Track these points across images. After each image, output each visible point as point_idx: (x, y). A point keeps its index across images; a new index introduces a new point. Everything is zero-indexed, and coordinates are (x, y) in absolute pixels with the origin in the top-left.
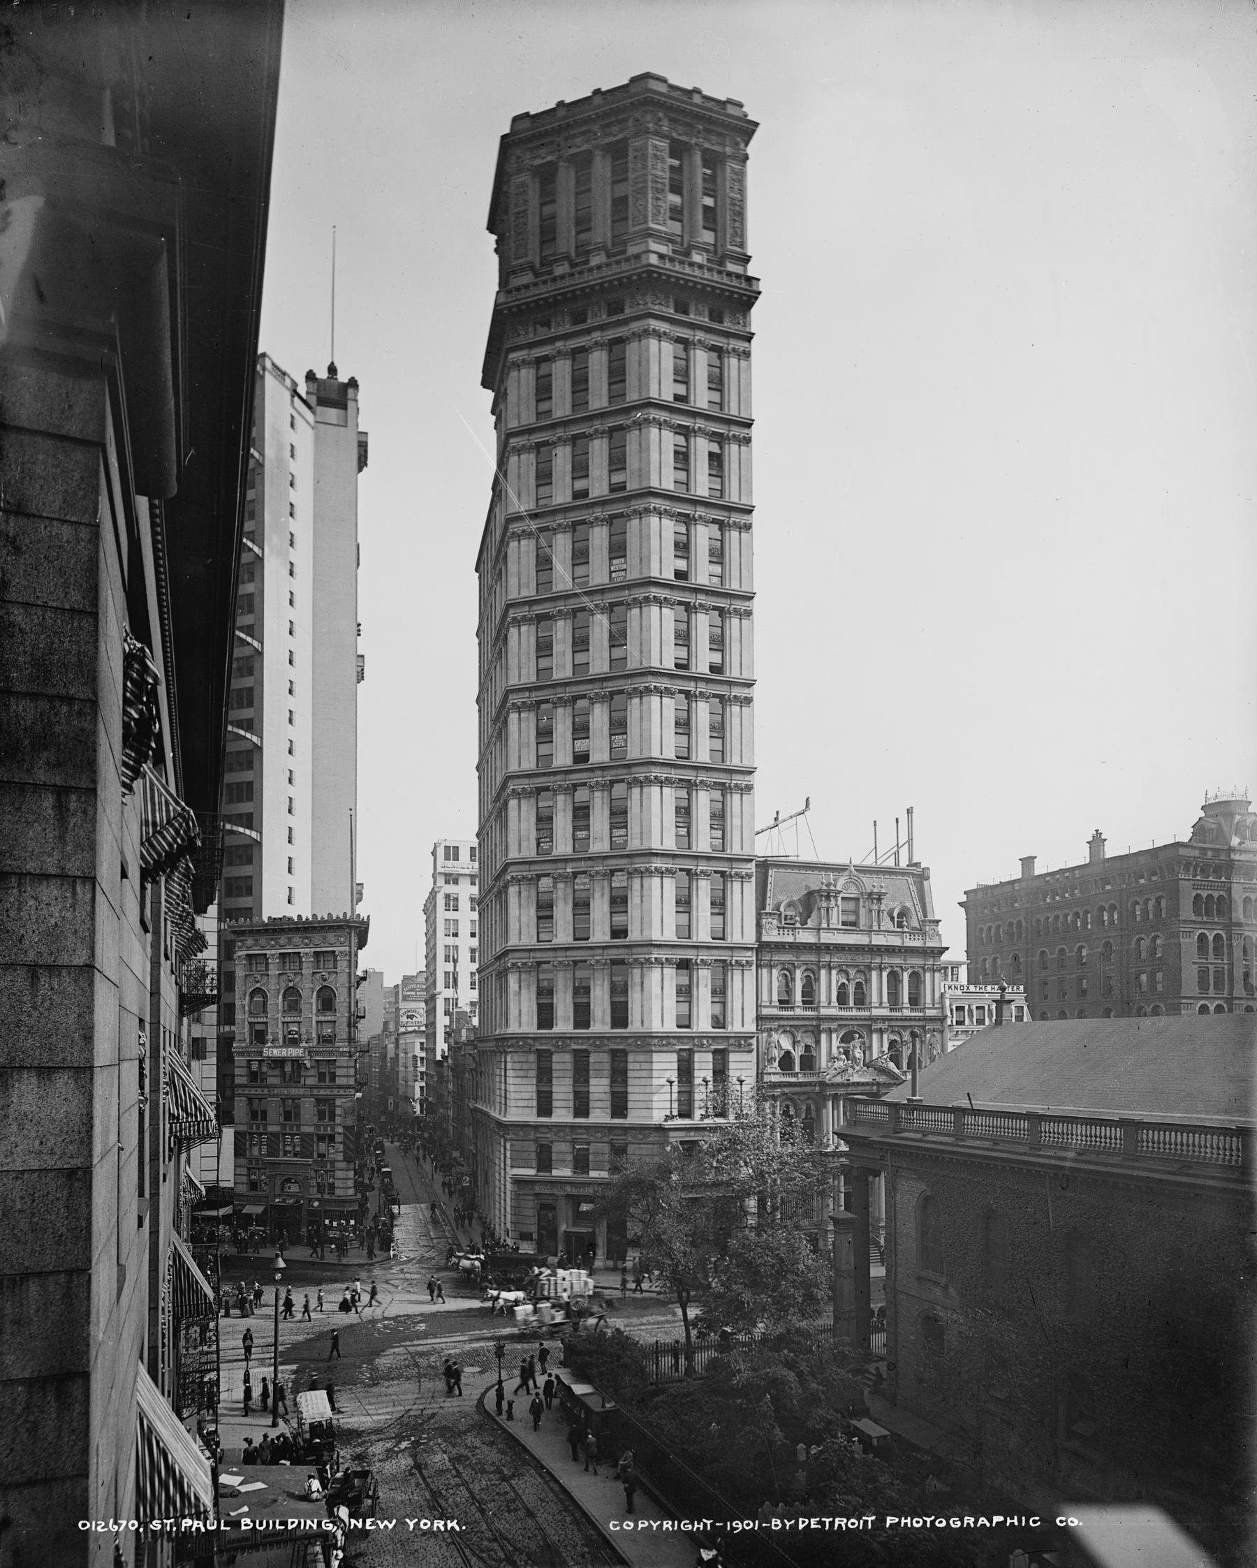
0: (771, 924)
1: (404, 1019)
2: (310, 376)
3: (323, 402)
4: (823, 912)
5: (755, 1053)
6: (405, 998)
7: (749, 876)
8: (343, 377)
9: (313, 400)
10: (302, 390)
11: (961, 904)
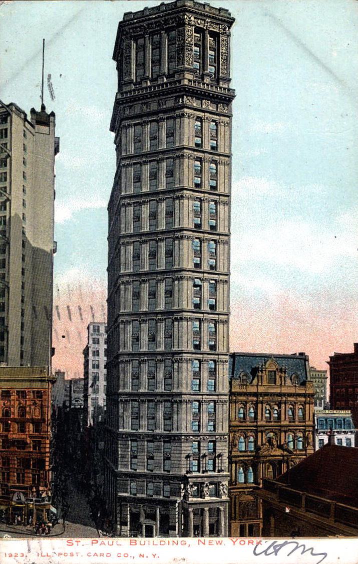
0: (236, 383)
1: (73, 402)
2: (33, 111)
3: (39, 123)
4: (260, 378)
5: (228, 442)
6: (74, 391)
7: (226, 362)
8: (48, 111)
9: (34, 122)
10: (29, 118)
11: (327, 362)
